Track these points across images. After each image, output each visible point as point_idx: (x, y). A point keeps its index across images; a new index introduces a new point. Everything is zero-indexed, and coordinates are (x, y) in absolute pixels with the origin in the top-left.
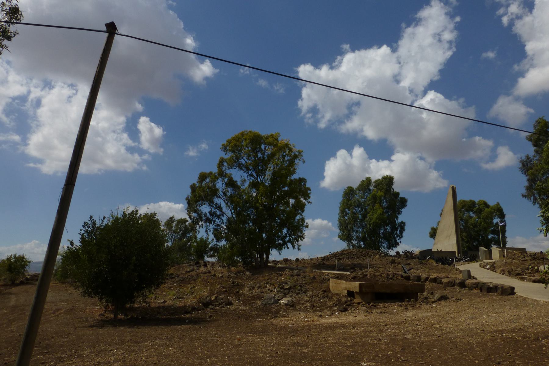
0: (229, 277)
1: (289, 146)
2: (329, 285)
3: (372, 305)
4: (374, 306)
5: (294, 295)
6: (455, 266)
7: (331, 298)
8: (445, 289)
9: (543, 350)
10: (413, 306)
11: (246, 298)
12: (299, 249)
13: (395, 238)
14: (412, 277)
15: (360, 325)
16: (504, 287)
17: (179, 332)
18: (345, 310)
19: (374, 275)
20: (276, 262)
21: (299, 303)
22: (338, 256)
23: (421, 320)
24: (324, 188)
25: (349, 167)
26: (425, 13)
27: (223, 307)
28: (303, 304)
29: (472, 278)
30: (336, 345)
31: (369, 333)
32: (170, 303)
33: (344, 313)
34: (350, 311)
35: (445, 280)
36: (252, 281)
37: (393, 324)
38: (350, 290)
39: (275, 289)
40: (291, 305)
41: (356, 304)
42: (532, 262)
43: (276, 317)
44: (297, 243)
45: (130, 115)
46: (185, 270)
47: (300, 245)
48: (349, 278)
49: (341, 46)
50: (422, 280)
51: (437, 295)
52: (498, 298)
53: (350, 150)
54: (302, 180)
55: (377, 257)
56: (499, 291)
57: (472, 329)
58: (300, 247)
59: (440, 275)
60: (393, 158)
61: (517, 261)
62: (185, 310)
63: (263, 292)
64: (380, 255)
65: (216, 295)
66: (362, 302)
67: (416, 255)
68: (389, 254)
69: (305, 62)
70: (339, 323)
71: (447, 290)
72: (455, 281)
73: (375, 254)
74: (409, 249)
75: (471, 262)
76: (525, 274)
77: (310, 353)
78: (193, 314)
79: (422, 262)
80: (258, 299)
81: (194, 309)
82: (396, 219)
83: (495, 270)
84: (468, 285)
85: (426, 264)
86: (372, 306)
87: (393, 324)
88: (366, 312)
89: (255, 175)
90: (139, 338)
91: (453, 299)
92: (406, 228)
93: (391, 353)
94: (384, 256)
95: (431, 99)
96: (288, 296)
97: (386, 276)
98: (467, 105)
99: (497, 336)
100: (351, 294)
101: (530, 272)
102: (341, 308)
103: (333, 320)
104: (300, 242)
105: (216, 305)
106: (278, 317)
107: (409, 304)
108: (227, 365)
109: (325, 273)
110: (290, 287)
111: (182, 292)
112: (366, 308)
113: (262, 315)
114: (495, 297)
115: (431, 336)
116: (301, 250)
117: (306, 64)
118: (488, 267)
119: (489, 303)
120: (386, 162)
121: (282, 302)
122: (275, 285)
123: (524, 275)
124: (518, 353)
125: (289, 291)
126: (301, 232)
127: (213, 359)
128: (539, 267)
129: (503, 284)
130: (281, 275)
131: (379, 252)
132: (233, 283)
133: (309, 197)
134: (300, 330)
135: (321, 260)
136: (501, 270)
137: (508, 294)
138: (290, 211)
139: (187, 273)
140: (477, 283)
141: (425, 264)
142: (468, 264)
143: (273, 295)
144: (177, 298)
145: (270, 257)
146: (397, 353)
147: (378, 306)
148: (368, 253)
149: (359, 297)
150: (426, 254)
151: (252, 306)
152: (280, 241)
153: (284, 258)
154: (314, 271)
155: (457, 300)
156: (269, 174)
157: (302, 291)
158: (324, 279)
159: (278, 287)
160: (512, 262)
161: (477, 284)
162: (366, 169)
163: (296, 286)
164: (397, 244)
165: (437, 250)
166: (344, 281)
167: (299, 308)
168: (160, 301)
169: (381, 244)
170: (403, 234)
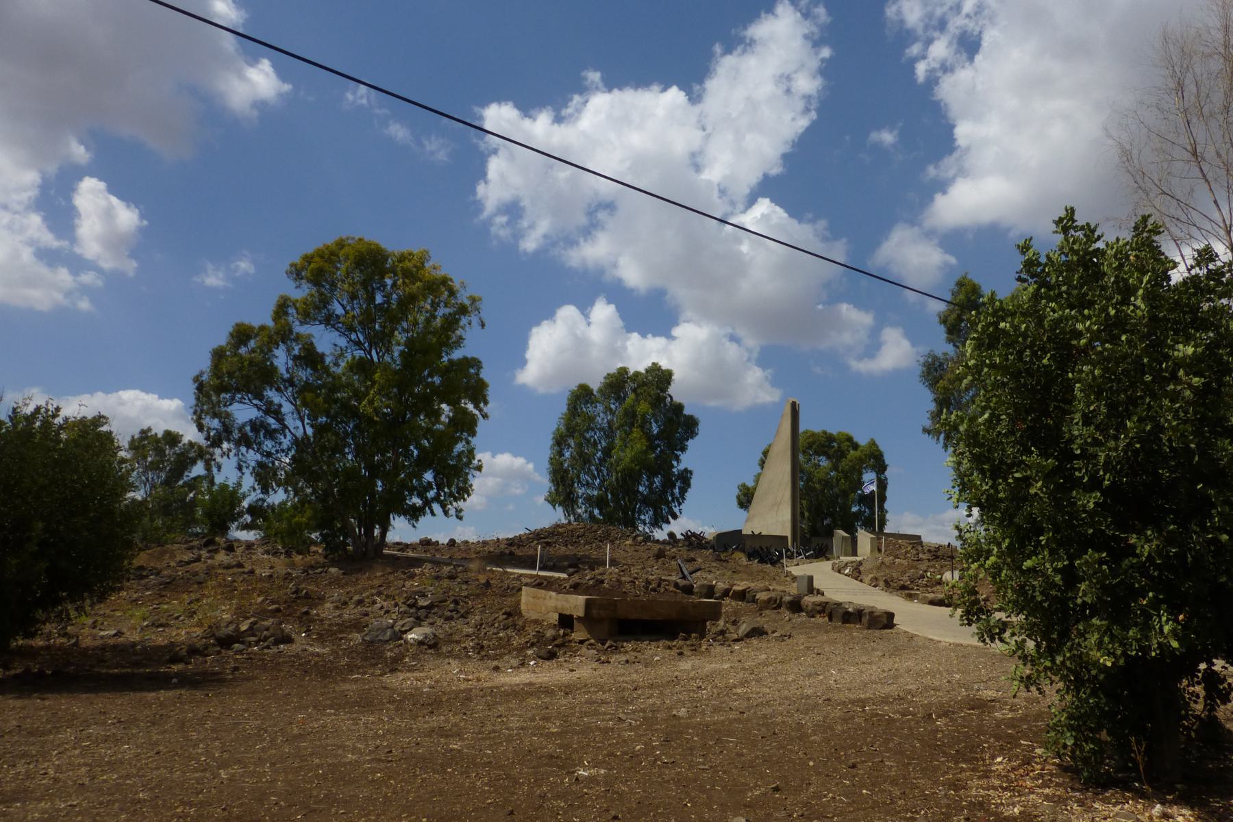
0: (285, 579)
1: (450, 283)
5: (440, 622)
7: (521, 630)
8: (761, 614)
10: (694, 648)
11: (326, 627)
12: (460, 518)
13: (668, 503)
15: (580, 689)
18: (551, 656)
19: (618, 581)
20: (403, 547)
21: (449, 639)
22: (544, 538)
24: (524, 386)
25: (580, 344)
26: (762, 29)
27: (268, 647)
28: (458, 642)
29: (815, 592)
32: (135, 637)
33: (548, 663)
34: (561, 659)
35: (762, 596)
36: (342, 587)
37: (651, 686)
38: (564, 612)
40: (431, 645)
42: (932, 563)
45: (52, 169)
46: (178, 559)
49: (583, 74)
52: (862, 633)
53: (585, 307)
55: (627, 542)
56: (865, 620)
57: (808, 697)
60: (676, 332)
61: (903, 561)
62: (172, 654)
63: (366, 615)
65: (252, 619)
66: (588, 640)
67: (707, 543)
68: (653, 536)
69: (500, 99)
72: (781, 598)
73: (624, 536)
77: (465, 750)
78: (190, 663)
81: (193, 651)
86: (609, 647)
87: (651, 686)
90: (42, 723)
91: (775, 635)
94: (643, 541)
95: (763, 215)
98: (833, 234)
99: (854, 711)
100: (566, 621)
102: (543, 653)
103: (523, 677)
105: (250, 643)
106: (399, 671)
108: (267, 781)
109: (512, 574)
111: (167, 611)
114: (856, 631)
117: (503, 103)
118: (847, 571)
120: (660, 342)
121: (410, 637)
122: (397, 597)
124: (891, 745)
125: (429, 613)
126: (466, 481)
127: (233, 769)
129: (873, 607)
130: (412, 577)
134: (448, 700)
140: (824, 603)
143: (391, 621)
144: (153, 625)
146: (654, 748)
147: (622, 647)
150: (729, 542)
152: (417, 501)
157: (458, 612)
158: (508, 588)
163: (446, 601)
167: (449, 652)
168: (107, 633)
169: (639, 515)
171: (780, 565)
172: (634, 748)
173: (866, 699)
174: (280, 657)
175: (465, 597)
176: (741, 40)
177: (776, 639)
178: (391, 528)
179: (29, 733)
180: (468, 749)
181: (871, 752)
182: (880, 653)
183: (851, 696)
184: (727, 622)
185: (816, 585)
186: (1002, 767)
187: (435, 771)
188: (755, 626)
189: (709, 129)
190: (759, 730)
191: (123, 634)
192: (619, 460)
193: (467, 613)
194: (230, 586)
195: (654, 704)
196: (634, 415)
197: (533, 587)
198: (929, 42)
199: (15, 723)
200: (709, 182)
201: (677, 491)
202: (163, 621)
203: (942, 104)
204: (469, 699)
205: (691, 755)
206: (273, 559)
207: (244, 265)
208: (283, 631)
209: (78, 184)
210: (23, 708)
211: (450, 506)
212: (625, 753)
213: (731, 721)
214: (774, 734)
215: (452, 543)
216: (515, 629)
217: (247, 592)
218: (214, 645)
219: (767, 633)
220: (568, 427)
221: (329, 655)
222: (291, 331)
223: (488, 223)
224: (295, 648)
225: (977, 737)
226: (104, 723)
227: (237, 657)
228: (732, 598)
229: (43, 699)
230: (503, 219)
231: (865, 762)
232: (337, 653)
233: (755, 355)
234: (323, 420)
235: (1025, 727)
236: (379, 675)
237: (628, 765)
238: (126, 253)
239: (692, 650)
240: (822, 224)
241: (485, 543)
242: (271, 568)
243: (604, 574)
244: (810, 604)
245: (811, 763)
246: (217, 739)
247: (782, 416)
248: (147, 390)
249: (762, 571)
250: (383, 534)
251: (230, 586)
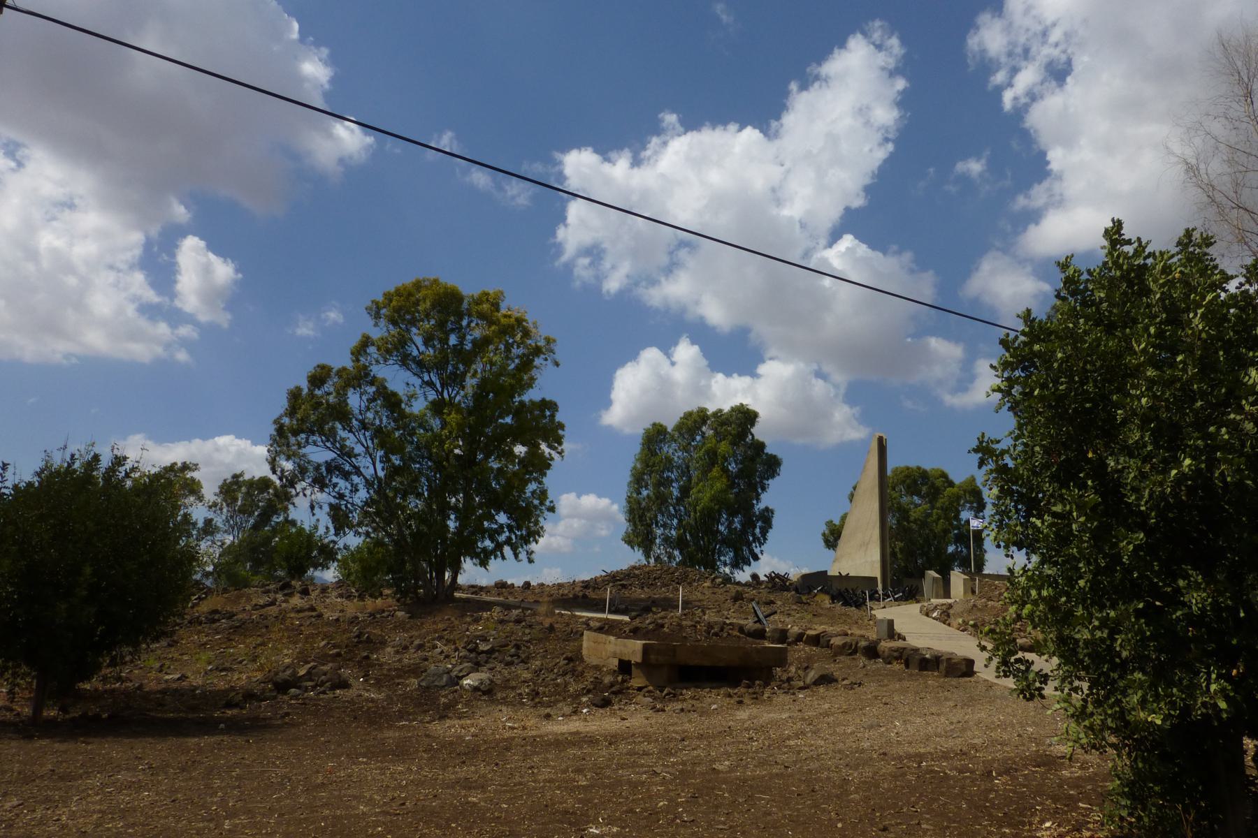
0: (352, 622)
1: (524, 323)
2: (581, 645)
3: (668, 694)
5: (499, 667)
7: (579, 676)
9: (987, 800)
10: (755, 696)
11: (385, 672)
13: (749, 545)
15: (626, 739)
17: (189, 752)
18: (606, 703)
19: (679, 625)
20: (477, 589)
21: (506, 685)
22: (620, 581)
23: (761, 729)
24: (610, 428)
25: (664, 385)
26: (834, 66)
27: (324, 693)
28: (513, 688)
29: (896, 637)
30: (552, 785)
31: (639, 758)
32: (196, 680)
33: (601, 711)
34: (616, 707)
35: (837, 641)
36: (407, 631)
37: (701, 737)
38: (624, 658)
39: (455, 652)
40: (486, 692)
41: (634, 689)
43: (442, 718)
44: (525, 546)
45: (154, 231)
46: (254, 602)
47: (532, 552)
48: (625, 632)
49: (660, 116)
50: (790, 640)
52: (937, 682)
53: (667, 347)
54: (548, 406)
55: (706, 584)
56: (943, 667)
57: (863, 751)
60: (763, 369)
62: (227, 699)
64: (713, 580)
65: (312, 664)
66: (646, 687)
68: (734, 578)
69: (578, 145)
70: (581, 733)
72: (857, 643)
73: (703, 578)
74: (782, 569)
77: (482, 804)
78: (245, 708)
80: (412, 675)
81: (249, 696)
82: (755, 502)
85: (809, 604)
86: (667, 694)
87: (701, 737)
88: (652, 709)
89: (438, 386)
90: (76, 767)
91: (845, 682)
92: (775, 521)
93: (664, 804)
94: (722, 583)
95: (848, 249)
96: (485, 669)
98: (921, 264)
99: (908, 767)
100: (625, 667)
102: (598, 700)
103: (575, 725)
104: (533, 546)
105: (306, 688)
106: (448, 718)
108: (266, 834)
109: (581, 617)
110: (492, 647)
111: (232, 655)
112: (651, 700)
113: (415, 713)
114: (932, 680)
115: (770, 765)
117: (583, 149)
118: (935, 615)
119: (917, 693)
120: (746, 380)
121: (465, 682)
122: (457, 642)
124: (935, 806)
125: (490, 658)
126: (537, 523)
127: (240, 819)
129: (952, 653)
130: (477, 621)
132: (358, 636)
133: (560, 443)
134: (486, 750)
137: (960, 674)
138: (515, 474)
139: (256, 610)
140: (901, 648)
143: (450, 666)
144: (217, 669)
145: (459, 576)
146: (678, 805)
147: (681, 694)
149: (641, 675)
150: (815, 582)
151: (396, 691)
152: (488, 544)
154: (557, 611)
155: (851, 686)
156: (471, 382)
157: (519, 657)
158: (572, 632)
162: (703, 391)
163: (507, 645)
166: (612, 638)
168: (171, 676)
169: (719, 557)
171: (864, 607)
172: (657, 804)
173: (924, 754)
174: (334, 703)
175: (527, 641)
176: (817, 78)
177: (845, 687)
178: (462, 571)
179: (60, 777)
180: (486, 802)
181: (910, 813)
182: (951, 704)
183: (910, 749)
184: (799, 668)
186: (1048, 833)
187: (438, 826)
188: (824, 673)
189: (788, 164)
190: (798, 787)
191: (187, 678)
192: (697, 500)
193: (528, 658)
194: (297, 630)
195: (699, 756)
196: (715, 453)
197: (595, 631)
198: (1015, 71)
199: (50, 767)
200: (791, 218)
201: (757, 531)
202: (227, 665)
203: (1032, 131)
204: (508, 749)
205: (715, 812)
206: (346, 602)
207: (333, 315)
208: (340, 676)
209: (182, 241)
210: (65, 752)
211: (520, 549)
212: (645, 810)
213: (772, 776)
214: (813, 791)
215: (527, 585)
217: (312, 636)
218: (271, 690)
219: (836, 681)
220: (646, 463)
221: (384, 700)
222: (367, 375)
223: (569, 267)
224: (350, 693)
225: (1033, 799)
226: (135, 769)
227: (293, 702)
228: (806, 643)
229: (88, 743)
230: (585, 261)
231: (901, 824)
232: (392, 699)
233: (842, 391)
234: (396, 460)
235: (1089, 787)
236: (427, 722)
237: (643, 823)
238: (222, 306)
240: (908, 256)
241: (560, 586)
242: (342, 611)
243: (666, 618)
244: (887, 650)
245: (840, 825)
246: (239, 787)
247: (869, 452)
248: (239, 437)
250: (454, 578)
251: (297, 630)
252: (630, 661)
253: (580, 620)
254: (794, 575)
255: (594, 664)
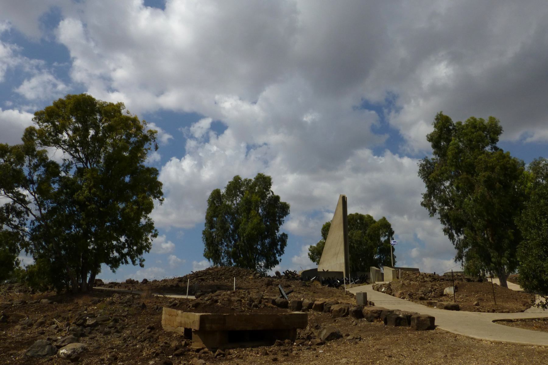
4: (221, 355)
6: (344, 289)
7: (152, 340)
8: (335, 321)
10: (286, 353)
12: (142, 266)
13: (275, 254)
14: (290, 303)
16: (421, 317)
19: (229, 300)
22: (200, 276)
35: (335, 308)
41: (194, 351)
42: (433, 283)
44: (139, 256)
47: (144, 260)
48: (189, 306)
50: (304, 308)
51: (324, 332)
55: (250, 277)
58: (144, 263)
59: (327, 300)
61: (416, 283)
66: (203, 348)
67: (297, 277)
68: (267, 274)
71: (337, 322)
72: (348, 309)
73: (249, 274)
75: (361, 284)
76: (429, 299)
79: (305, 283)
82: (276, 231)
83: (393, 294)
84: (367, 314)
85: (310, 287)
94: (260, 276)
96: (87, 339)
97: (248, 302)
100: (188, 333)
101: (434, 296)
107: (280, 350)
109: (170, 298)
116: (144, 267)
118: (383, 290)
121: (61, 352)
123: (428, 299)
125: (93, 330)
128: (444, 289)
131: (254, 272)
135: (178, 281)
136: (400, 293)
140: (380, 311)
141: (308, 286)
142: (359, 286)
147: (229, 354)
148: (240, 273)
149: (200, 339)
153: (128, 278)
159: (74, 323)
160: (410, 284)
161: (379, 312)
163: (109, 320)
164: (276, 262)
165: (323, 271)
169: (258, 262)
170: (284, 249)
171: (341, 288)
175: (124, 316)
184: (312, 327)
185: (369, 299)
201: (279, 247)
211: (136, 258)
216: (150, 341)
219: (341, 336)
239: (285, 355)
243: (220, 295)
249: (331, 291)
252: (191, 329)
253: (169, 300)
254: (299, 272)
255: (169, 331)
